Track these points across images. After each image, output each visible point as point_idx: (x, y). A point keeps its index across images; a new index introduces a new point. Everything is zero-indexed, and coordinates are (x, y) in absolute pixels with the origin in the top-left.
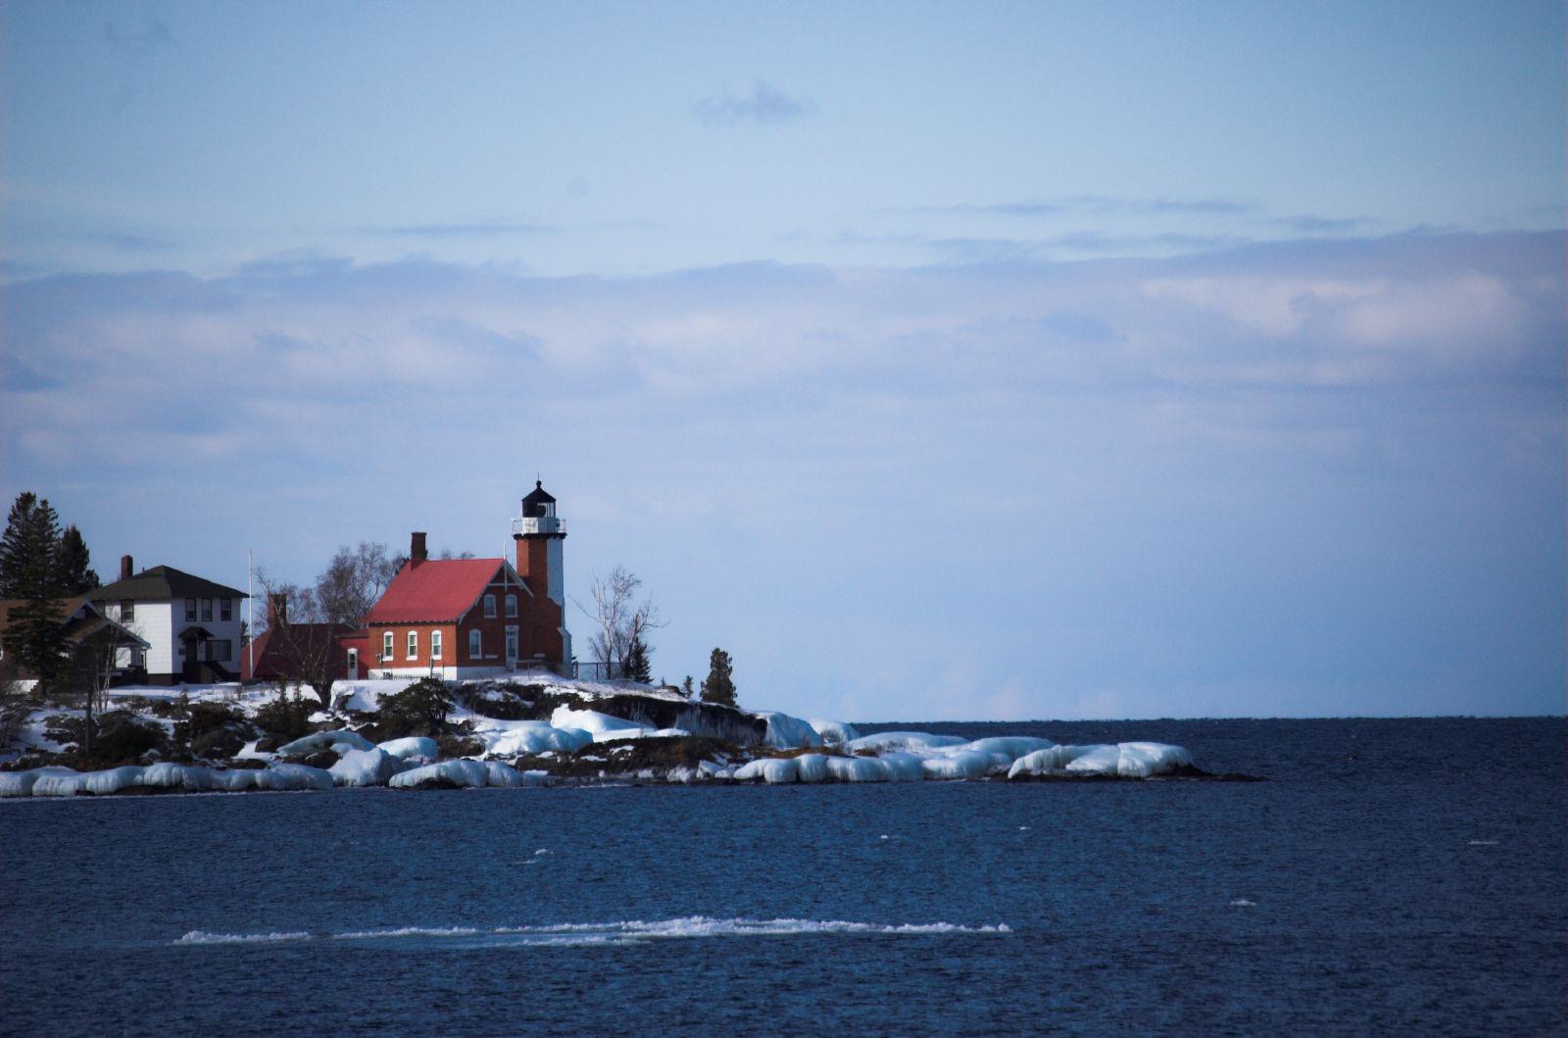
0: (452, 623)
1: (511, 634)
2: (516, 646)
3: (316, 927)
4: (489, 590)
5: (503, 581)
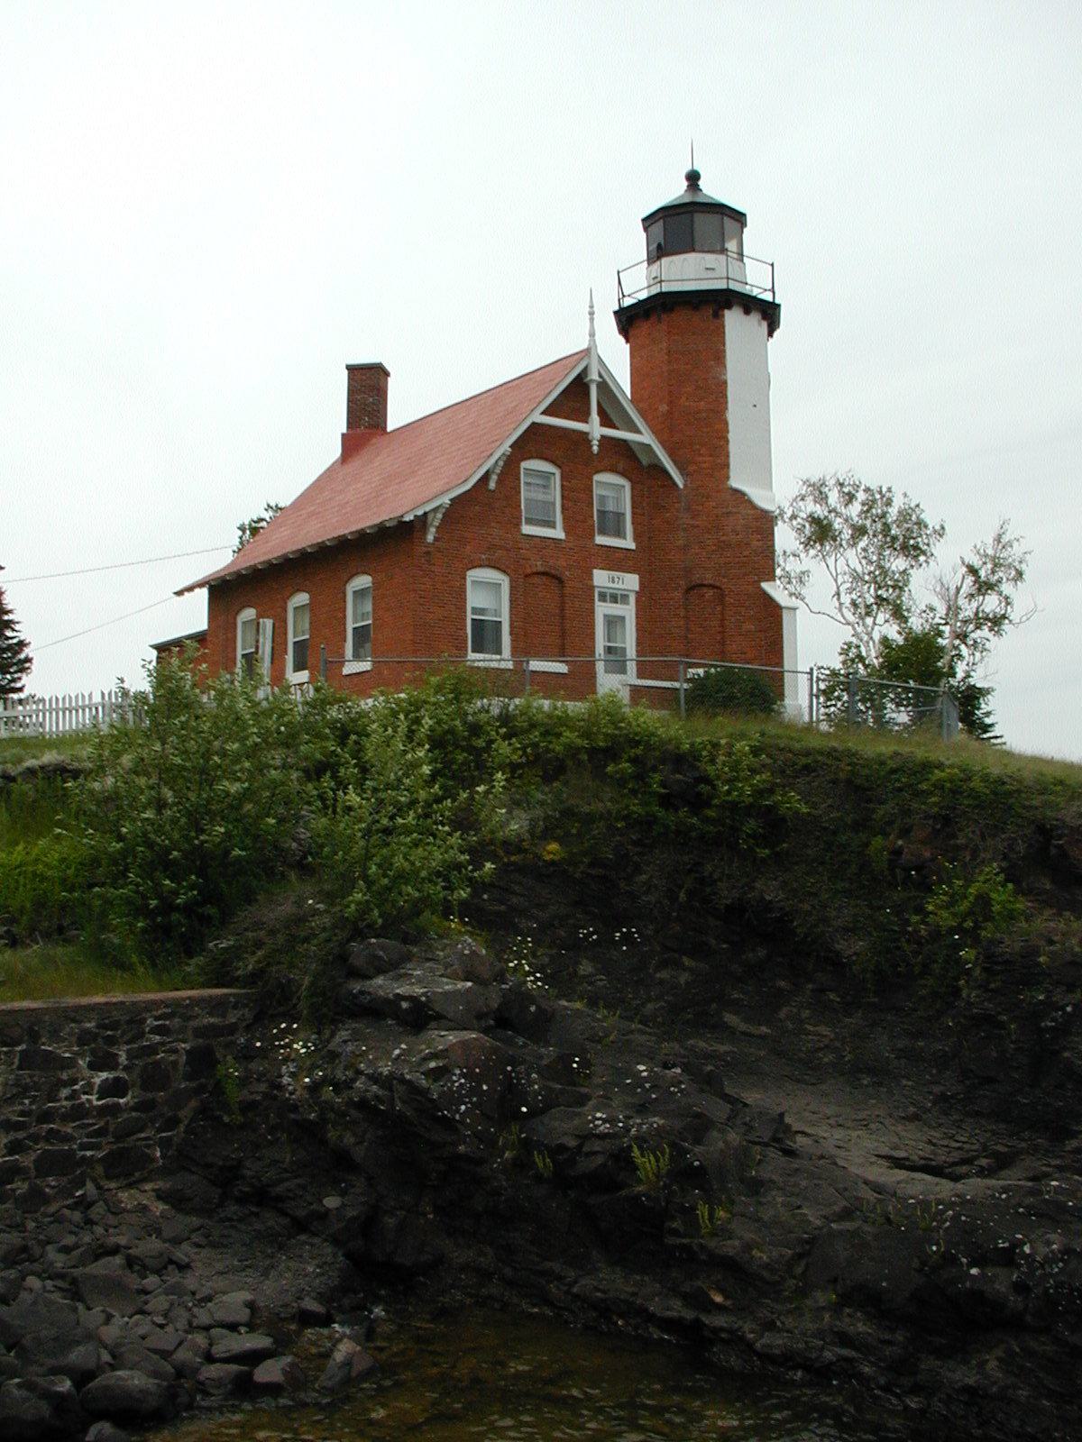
0: (200, 585)
1: (614, 599)
2: (629, 640)
3: (141, 1035)
4: (534, 441)
5: (606, 421)
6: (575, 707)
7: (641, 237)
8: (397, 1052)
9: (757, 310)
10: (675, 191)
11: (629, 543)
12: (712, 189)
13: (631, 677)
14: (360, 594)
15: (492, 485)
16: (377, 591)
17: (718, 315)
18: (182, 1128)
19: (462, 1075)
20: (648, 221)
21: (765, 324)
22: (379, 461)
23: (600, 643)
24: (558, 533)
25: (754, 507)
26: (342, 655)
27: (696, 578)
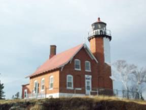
2: (90, 85)
7: (91, 27)
10: (96, 21)
11: (90, 71)
12: (102, 20)
13: (91, 90)
17: (102, 38)
20: (92, 25)
22: (55, 58)
23: (86, 85)
24: (80, 70)
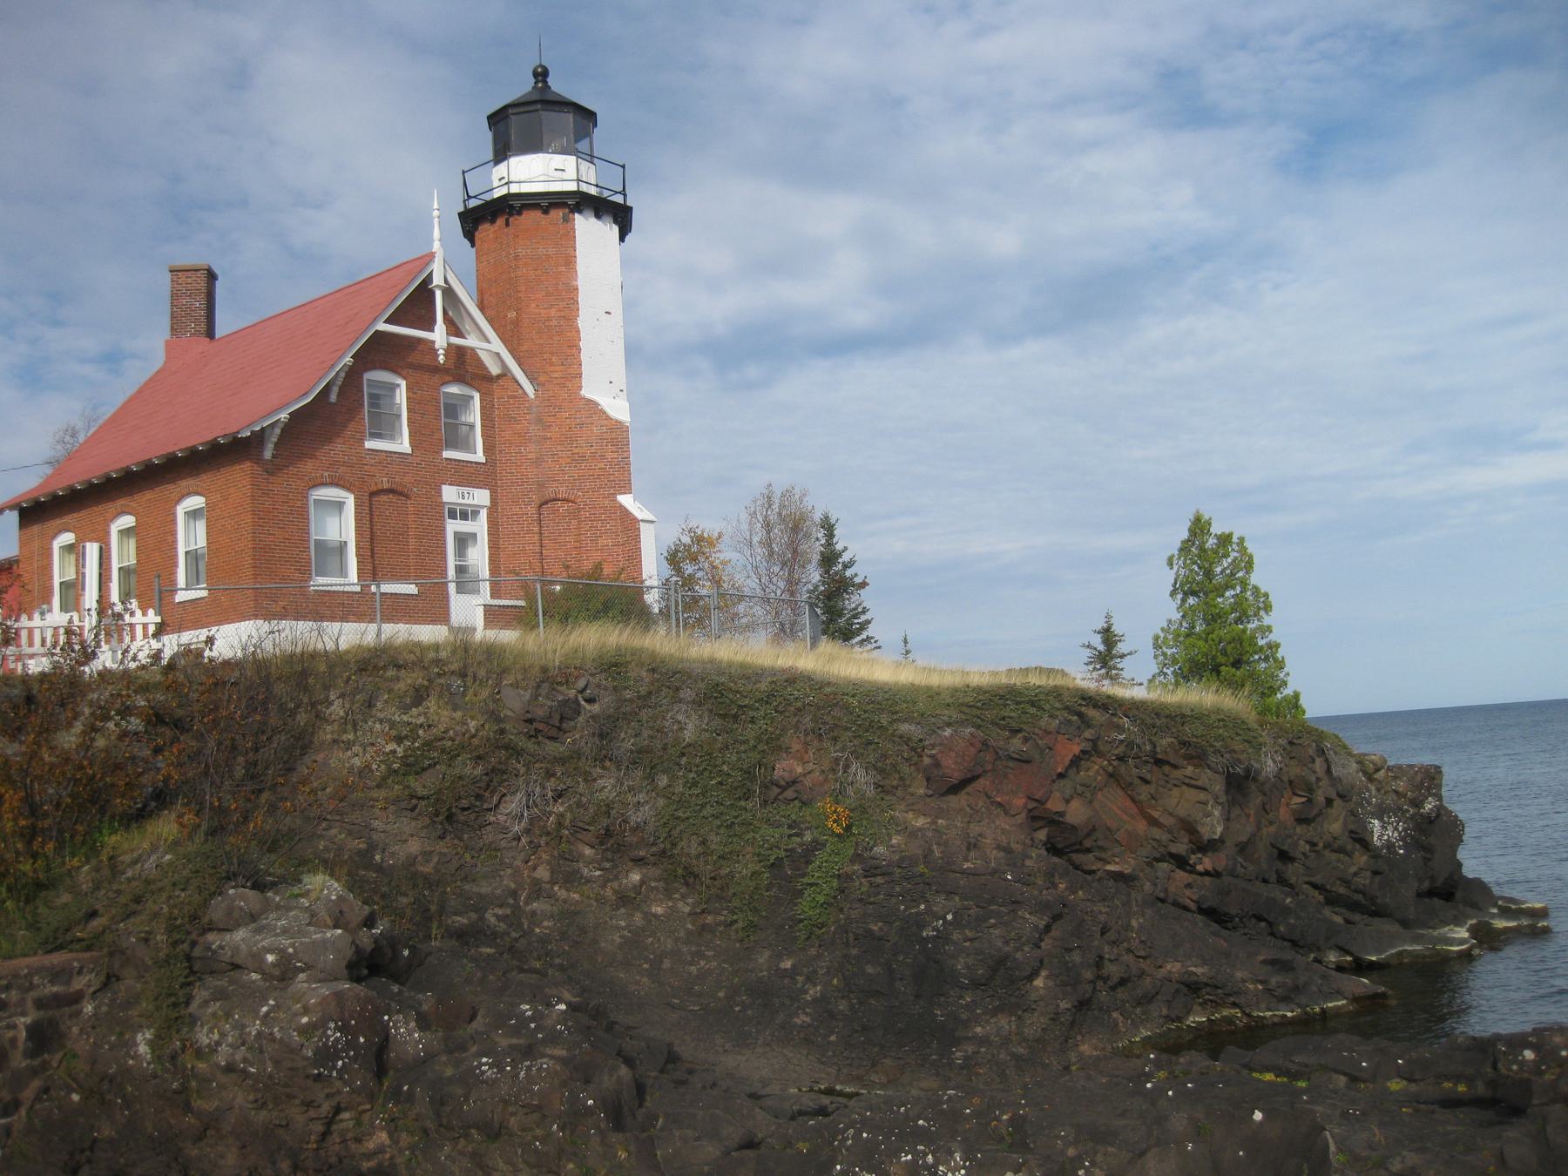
2: (479, 556)
6: (427, 633)
8: (265, 1009)
9: (589, 207)
14: (193, 515)
15: (333, 398)
16: (208, 514)
18: (23, 1112)
19: (337, 1028)
21: (616, 229)
25: (608, 418)
26: (174, 582)
27: (549, 492)
